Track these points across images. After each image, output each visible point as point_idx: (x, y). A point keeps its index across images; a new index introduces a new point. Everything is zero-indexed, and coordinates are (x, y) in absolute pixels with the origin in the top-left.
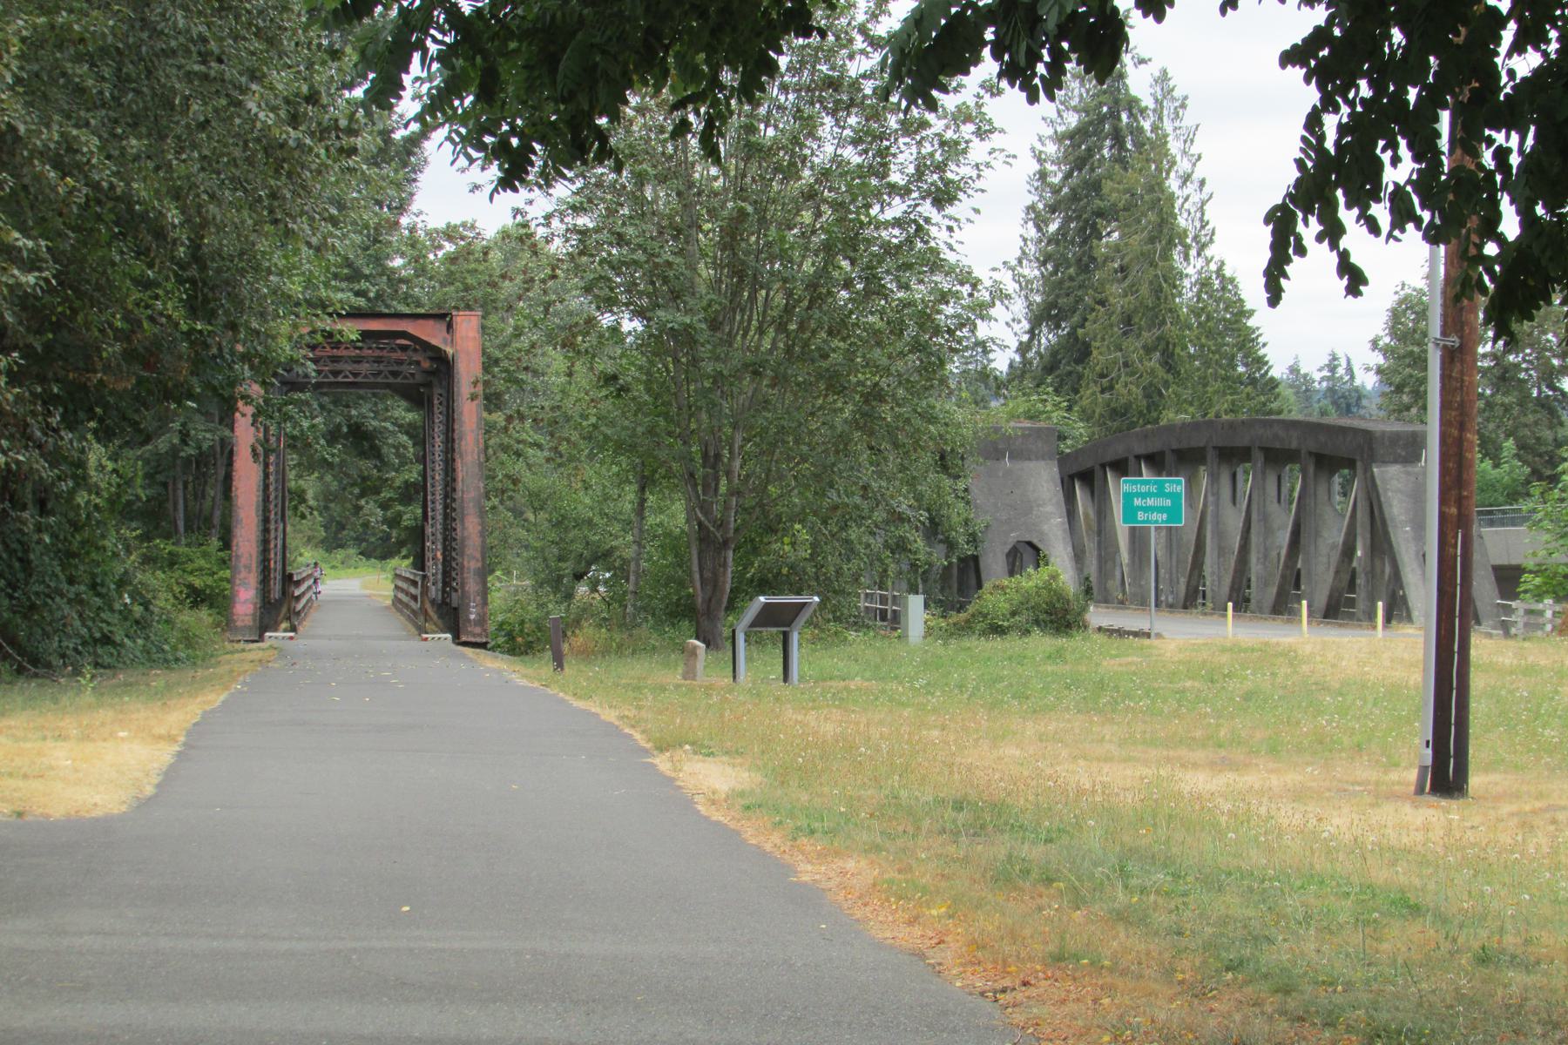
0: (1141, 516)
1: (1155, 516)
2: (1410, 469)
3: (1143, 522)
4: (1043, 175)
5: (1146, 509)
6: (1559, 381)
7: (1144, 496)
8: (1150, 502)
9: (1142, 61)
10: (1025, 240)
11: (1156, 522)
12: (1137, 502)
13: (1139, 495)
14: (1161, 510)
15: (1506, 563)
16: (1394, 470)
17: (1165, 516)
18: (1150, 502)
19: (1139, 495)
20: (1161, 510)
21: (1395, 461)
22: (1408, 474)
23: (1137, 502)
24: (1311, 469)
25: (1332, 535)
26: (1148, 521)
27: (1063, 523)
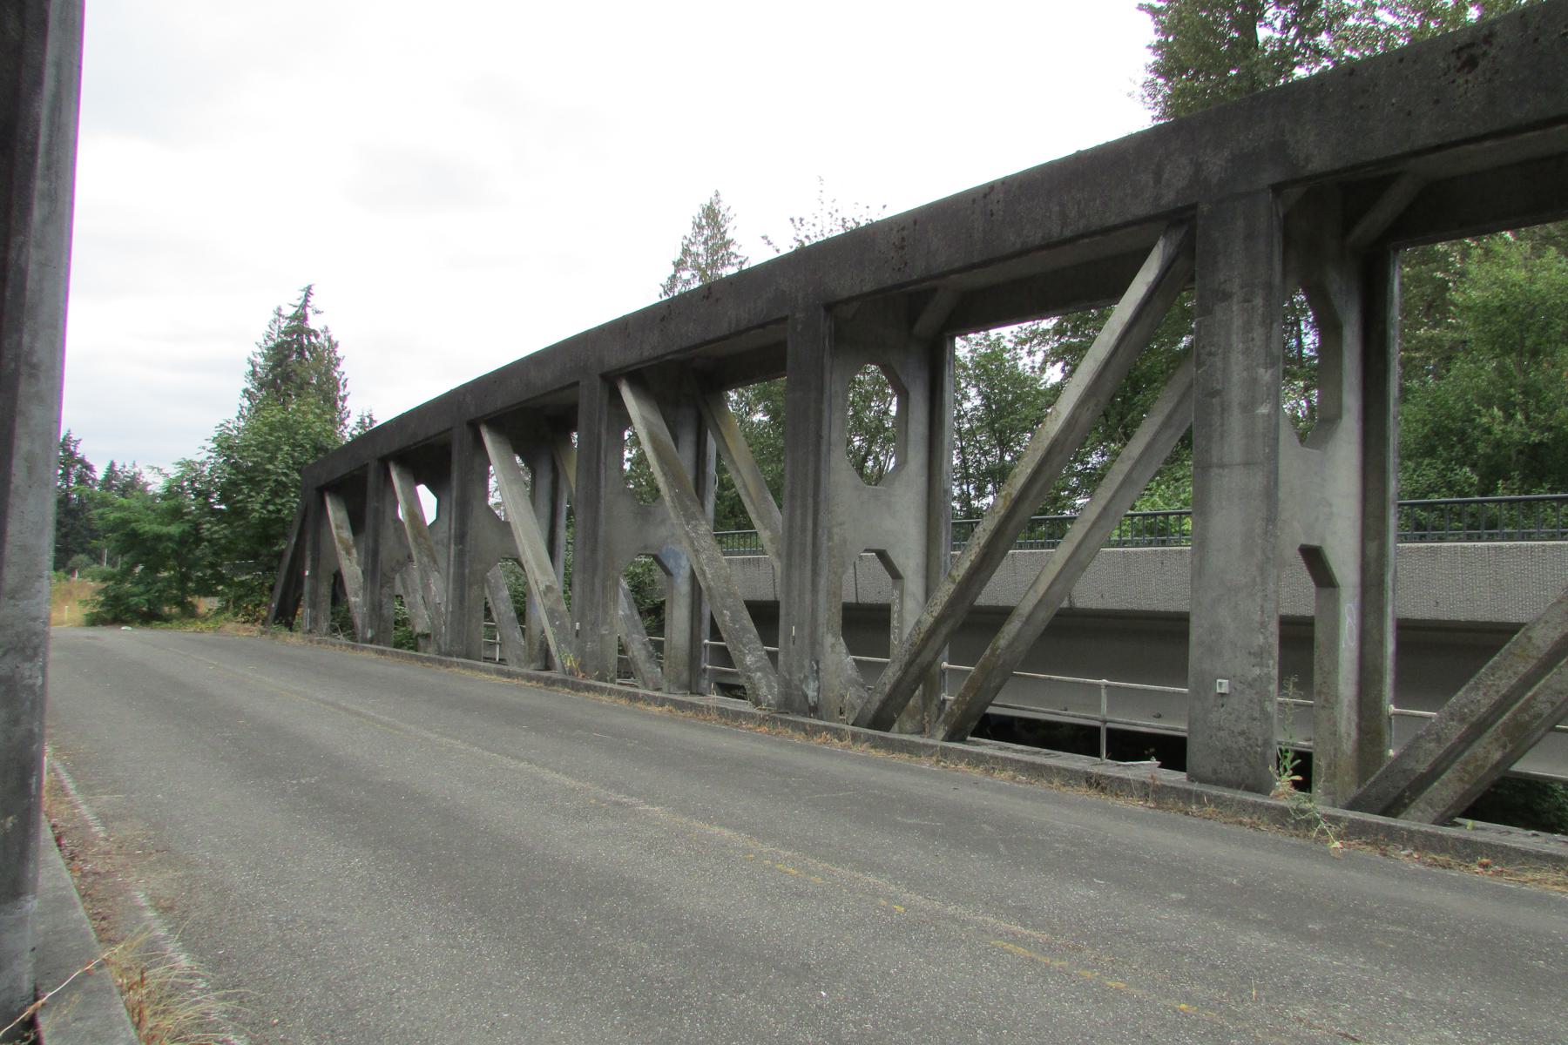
9: (317, 312)
10: (242, 407)
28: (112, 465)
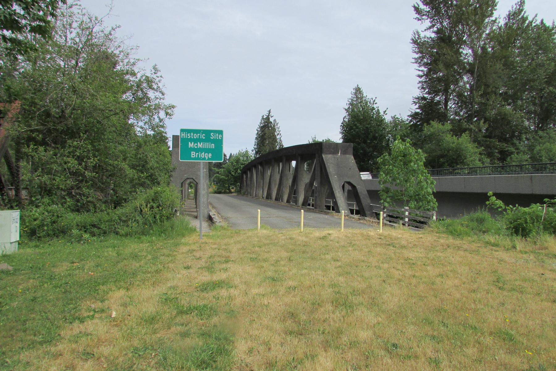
0: (193, 154)
1: (203, 155)
2: (335, 156)
3: (195, 159)
4: (258, 133)
5: (197, 150)
6: (549, 27)
7: (196, 141)
8: (200, 145)
11: (204, 159)
12: (191, 145)
13: (191, 140)
14: (207, 151)
15: (530, 193)
16: (330, 156)
17: (210, 155)
18: (200, 145)
19: (191, 140)
20: (207, 151)
21: (330, 154)
22: (335, 158)
23: (191, 145)
24: (299, 159)
25: (305, 179)
26: (198, 158)
27: (206, 171)
28: (231, 154)
